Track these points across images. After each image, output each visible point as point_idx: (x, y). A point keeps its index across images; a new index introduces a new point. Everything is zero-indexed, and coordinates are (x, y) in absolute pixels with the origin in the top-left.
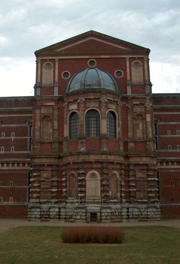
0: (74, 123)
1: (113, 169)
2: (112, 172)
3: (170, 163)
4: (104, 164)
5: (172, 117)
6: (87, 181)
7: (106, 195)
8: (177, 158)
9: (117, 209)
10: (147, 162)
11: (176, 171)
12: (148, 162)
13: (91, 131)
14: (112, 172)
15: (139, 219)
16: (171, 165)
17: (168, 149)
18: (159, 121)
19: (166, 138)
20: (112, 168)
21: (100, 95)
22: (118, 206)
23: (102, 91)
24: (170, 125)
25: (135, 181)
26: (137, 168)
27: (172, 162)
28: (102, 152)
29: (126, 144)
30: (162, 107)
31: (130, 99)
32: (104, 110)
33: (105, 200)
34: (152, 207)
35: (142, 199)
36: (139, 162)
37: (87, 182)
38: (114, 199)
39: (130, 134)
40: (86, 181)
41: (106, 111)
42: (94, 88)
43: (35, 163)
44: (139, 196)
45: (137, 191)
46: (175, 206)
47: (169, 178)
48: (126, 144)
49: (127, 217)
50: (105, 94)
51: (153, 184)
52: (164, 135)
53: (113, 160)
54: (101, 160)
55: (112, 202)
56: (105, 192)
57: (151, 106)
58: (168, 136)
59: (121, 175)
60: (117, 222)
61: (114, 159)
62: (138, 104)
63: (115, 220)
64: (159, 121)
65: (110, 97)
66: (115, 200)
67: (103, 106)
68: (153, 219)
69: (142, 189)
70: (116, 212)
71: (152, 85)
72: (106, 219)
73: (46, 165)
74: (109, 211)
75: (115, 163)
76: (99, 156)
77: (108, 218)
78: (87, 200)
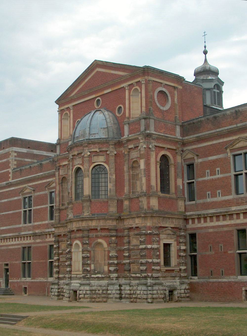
0: (81, 180)
1: (97, 237)
2: (96, 241)
3: (221, 218)
4: (85, 232)
5: (212, 148)
6: (73, 253)
7: (86, 269)
8: (216, 210)
9: (101, 286)
10: (139, 224)
11: (231, 229)
12: (140, 225)
13: (102, 186)
14: (96, 241)
15: (132, 300)
16: (210, 222)
17: (206, 198)
18: (195, 158)
19: (204, 181)
20: (95, 236)
21: (82, 149)
22: (104, 282)
23: (83, 144)
24: (209, 161)
25: (129, 250)
26: (132, 233)
27: (223, 216)
28: (80, 219)
29: (120, 203)
30: (197, 137)
31: (125, 143)
32: (86, 166)
33: (84, 275)
34: (141, 284)
35: (136, 274)
36: (132, 225)
37: (73, 254)
38: (97, 274)
39: (126, 189)
40: (72, 252)
41: (90, 166)
42: (80, 140)
43: (90, 227)
44: (134, 270)
45: (132, 263)
46: (213, 282)
47: (208, 241)
48: (120, 203)
49: (118, 296)
50: (87, 146)
51: (144, 253)
52: (202, 177)
53: (96, 226)
54: (82, 228)
55: (94, 278)
56: (85, 266)
57: (145, 148)
58: (206, 178)
59: (109, 244)
60: (101, 302)
61: (97, 225)
62: (132, 148)
63: (97, 300)
64: (195, 158)
65: (94, 148)
66: (100, 276)
67: (85, 162)
68: (143, 300)
69: (136, 260)
70: (99, 290)
71: (223, 92)
72: (84, 298)
73: (99, 228)
74: (87, 288)
75: (98, 230)
76: (80, 223)
77: (86, 297)
78: (72, 276)
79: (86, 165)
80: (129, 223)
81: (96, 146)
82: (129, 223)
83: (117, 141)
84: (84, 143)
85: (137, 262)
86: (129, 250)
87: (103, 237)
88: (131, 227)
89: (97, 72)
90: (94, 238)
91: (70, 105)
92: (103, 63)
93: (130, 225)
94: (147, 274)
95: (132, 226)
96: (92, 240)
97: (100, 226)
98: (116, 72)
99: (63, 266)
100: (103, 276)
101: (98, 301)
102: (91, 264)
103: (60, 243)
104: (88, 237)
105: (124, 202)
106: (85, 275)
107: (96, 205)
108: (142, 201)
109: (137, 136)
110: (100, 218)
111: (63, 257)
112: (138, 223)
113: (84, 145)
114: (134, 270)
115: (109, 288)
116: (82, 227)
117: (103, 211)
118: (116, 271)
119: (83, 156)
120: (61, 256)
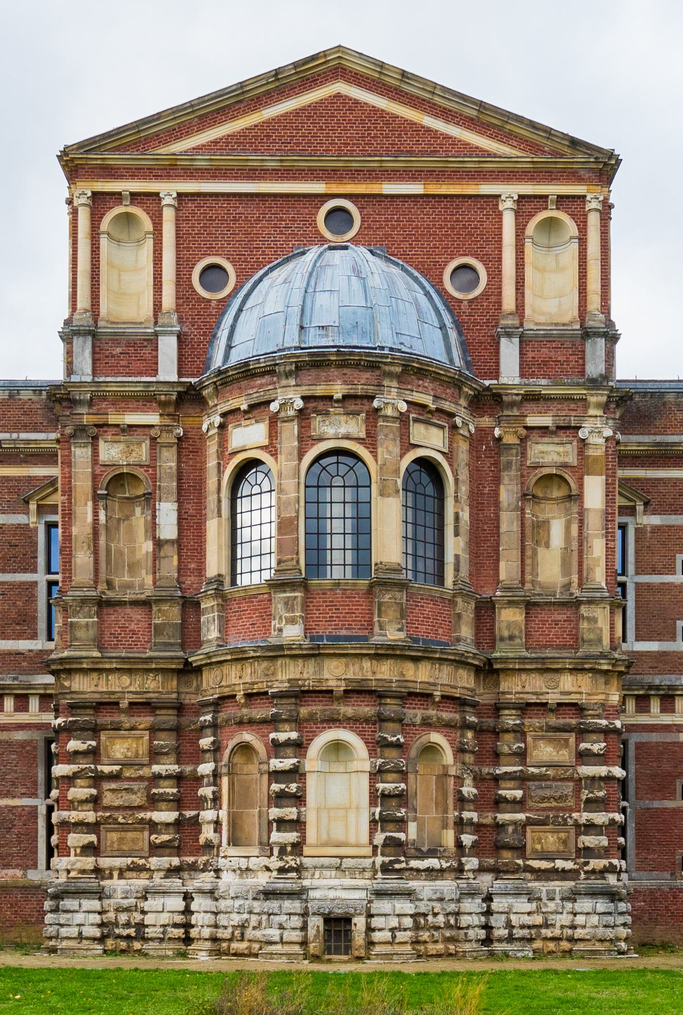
1: (427, 724)
2: (424, 739)
14: (424, 739)
23: (385, 364)
25: (522, 779)
26: (534, 722)
29: (485, 611)
31: (512, 405)
35: (553, 860)
36: (542, 694)
44: (538, 847)
48: (485, 611)
55: (418, 870)
59: (460, 751)
61: (432, 680)
68: (597, 944)
70: (435, 915)
74: (405, 906)
75: (437, 700)
76: (367, 664)
79: (387, 448)
80: (514, 687)
81: (426, 384)
82: (514, 687)
83: (481, 387)
84: (389, 360)
85: (560, 820)
86: (522, 779)
87: (444, 726)
88: (538, 701)
89: (338, 96)
90: (415, 726)
91: (168, 190)
92: (380, 73)
93: (535, 694)
94: (610, 863)
95: (541, 697)
96: (409, 733)
97: (441, 685)
98: (449, 126)
99: (122, 824)
100: (445, 865)
101: (434, 952)
102: (407, 822)
103: (103, 736)
104: (400, 721)
105: (500, 613)
106: (392, 858)
107: (325, 602)
108: (595, 620)
109: (585, 392)
110: (223, 658)
111: (125, 789)
112: (575, 689)
113: (387, 368)
114: (542, 848)
115: (147, 905)
116: (376, 680)
117: (440, 631)
118: (477, 849)
119: (377, 410)
120: (106, 786)
